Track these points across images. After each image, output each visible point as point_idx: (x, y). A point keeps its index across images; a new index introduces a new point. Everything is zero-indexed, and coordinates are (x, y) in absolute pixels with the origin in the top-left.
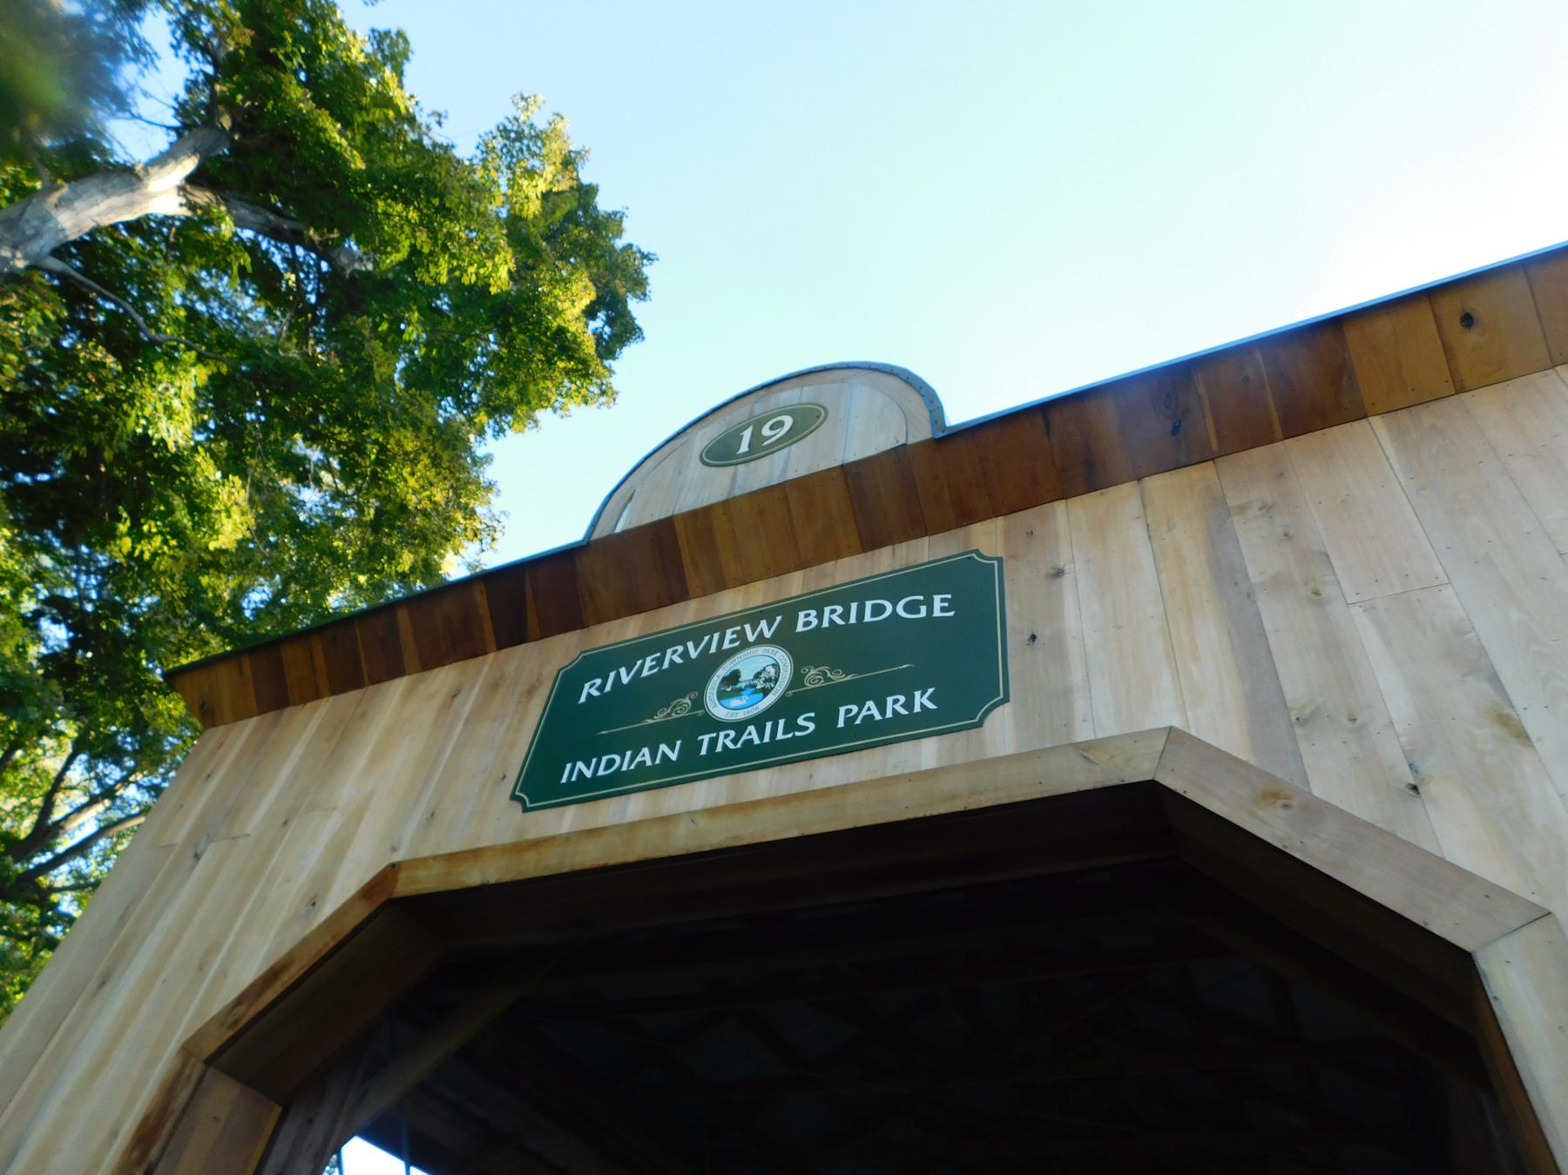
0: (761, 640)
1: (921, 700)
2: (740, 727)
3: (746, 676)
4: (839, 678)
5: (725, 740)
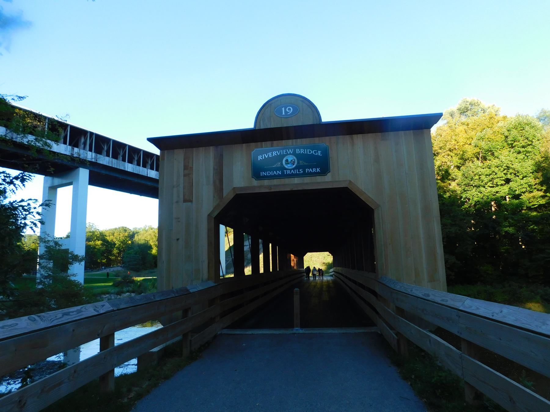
0: (290, 154)
1: (318, 170)
2: (291, 170)
3: (289, 160)
4: (305, 164)
5: (288, 172)
